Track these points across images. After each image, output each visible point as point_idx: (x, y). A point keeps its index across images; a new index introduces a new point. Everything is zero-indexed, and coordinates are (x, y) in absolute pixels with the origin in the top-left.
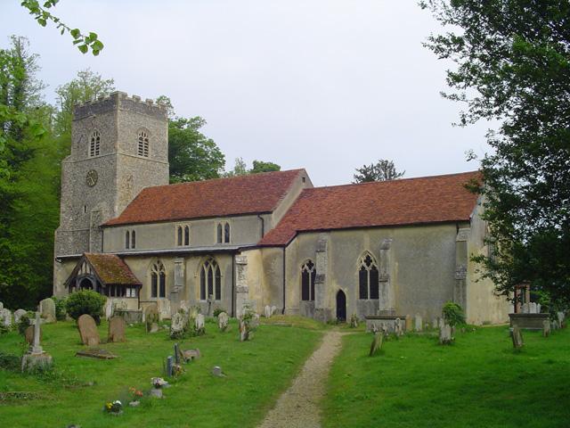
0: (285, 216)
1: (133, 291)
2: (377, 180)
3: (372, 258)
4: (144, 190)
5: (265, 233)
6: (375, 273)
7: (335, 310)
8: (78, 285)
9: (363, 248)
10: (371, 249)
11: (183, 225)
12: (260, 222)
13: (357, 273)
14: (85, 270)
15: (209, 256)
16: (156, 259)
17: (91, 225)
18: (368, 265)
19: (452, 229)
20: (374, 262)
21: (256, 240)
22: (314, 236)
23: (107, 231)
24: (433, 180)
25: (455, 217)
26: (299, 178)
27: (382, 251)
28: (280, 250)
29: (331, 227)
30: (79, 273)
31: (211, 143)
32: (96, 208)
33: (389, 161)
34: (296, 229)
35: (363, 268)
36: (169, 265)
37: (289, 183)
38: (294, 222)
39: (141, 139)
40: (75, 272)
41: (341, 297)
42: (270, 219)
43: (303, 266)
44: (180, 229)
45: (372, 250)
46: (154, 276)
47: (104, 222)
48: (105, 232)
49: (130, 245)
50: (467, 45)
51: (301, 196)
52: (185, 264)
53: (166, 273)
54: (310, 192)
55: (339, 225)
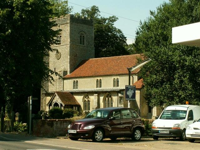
1: (76, 108)
11: (99, 78)
31: (120, 31)
39: (81, 36)
50: (142, 25)
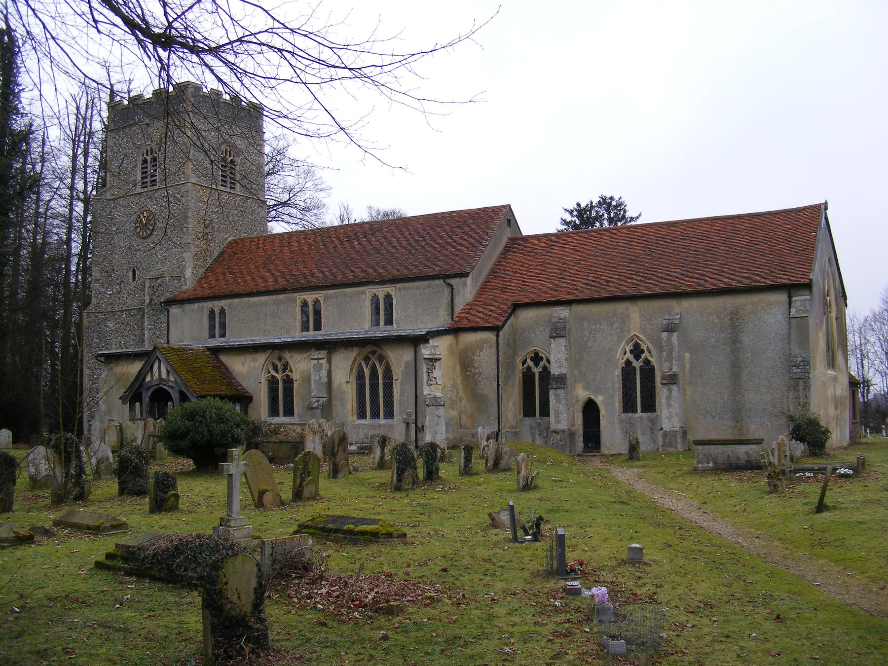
0: (487, 281)
2: (599, 224)
3: (644, 347)
4: (231, 243)
5: (457, 310)
6: (648, 371)
7: (581, 433)
8: (146, 399)
9: (629, 331)
10: (643, 331)
12: (447, 291)
13: (618, 372)
14: (160, 372)
15: (370, 347)
16: (277, 353)
17: (147, 302)
18: (637, 357)
19: (781, 297)
20: (646, 353)
21: (442, 320)
22: (544, 312)
23: (175, 310)
24: (640, 232)
25: (784, 280)
26: (501, 219)
27: (665, 335)
28: (490, 336)
29: (573, 297)
30: (148, 379)
32: (154, 273)
33: (616, 198)
34: (511, 301)
35: (628, 363)
36: (300, 365)
37: (487, 228)
38: (504, 290)
40: (141, 375)
41: (591, 410)
42: (465, 284)
43: (524, 362)
44: (212, 312)
45: (644, 335)
46: (273, 383)
47: (167, 295)
48: (171, 311)
49: (217, 332)
51: (507, 249)
52: (329, 362)
53: (295, 376)
54: (519, 242)
55: (586, 295)
